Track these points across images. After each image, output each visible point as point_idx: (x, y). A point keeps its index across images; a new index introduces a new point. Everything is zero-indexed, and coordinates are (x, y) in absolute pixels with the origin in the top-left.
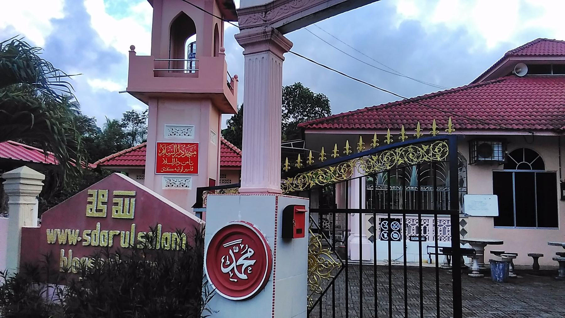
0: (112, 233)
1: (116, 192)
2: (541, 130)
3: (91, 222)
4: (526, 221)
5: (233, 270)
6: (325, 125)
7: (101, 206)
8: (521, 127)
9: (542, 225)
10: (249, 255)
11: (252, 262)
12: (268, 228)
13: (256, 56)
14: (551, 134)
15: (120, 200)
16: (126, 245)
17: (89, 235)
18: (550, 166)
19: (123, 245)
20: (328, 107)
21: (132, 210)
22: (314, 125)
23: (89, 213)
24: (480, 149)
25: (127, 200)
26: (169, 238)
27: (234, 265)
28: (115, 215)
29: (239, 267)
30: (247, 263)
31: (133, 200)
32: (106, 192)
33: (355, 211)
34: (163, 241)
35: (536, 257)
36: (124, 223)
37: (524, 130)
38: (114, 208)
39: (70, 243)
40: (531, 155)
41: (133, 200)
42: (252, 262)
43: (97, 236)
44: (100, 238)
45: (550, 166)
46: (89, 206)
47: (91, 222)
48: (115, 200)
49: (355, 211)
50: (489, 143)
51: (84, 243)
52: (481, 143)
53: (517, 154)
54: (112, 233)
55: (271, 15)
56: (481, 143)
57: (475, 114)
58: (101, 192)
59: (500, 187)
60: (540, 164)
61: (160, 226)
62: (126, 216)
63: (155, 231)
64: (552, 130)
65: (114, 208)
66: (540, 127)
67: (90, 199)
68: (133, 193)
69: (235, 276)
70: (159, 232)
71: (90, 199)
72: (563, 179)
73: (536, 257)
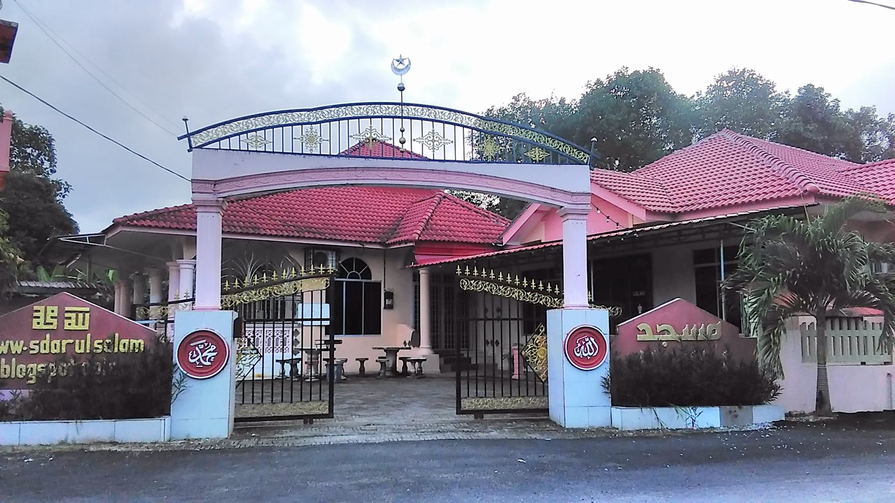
0: (64, 342)
1: (67, 309)
2: (370, 243)
3: (39, 334)
4: (354, 330)
5: (199, 360)
6: (149, 222)
7: (49, 320)
8: (354, 239)
9: (368, 332)
10: (212, 349)
11: (215, 354)
12: (225, 331)
13: (207, 214)
14: (378, 247)
15: (73, 315)
16: (82, 351)
17: (38, 344)
18: (376, 276)
19: (77, 351)
20: (52, 150)
21: (87, 323)
22: (135, 222)
23: (35, 326)
24: (315, 255)
25: (81, 315)
26: (127, 343)
27: (200, 356)
28: (67, 327)
29: (204, 358)
30: (210, 355)
31: (87, 315)
32: (55, 308)
33: (481, 319)
34: (121, 346)
35: (362, 361)
36: (81, 334)
37: (356, 242)
38: (67, 322)
39: (14, 352)
40: (361, 264)
41: (87, 315)
42: (215, 354)
43: (48, 345)
44: (57, 346)
45: (376, 276)
46: (35, 321)
47: (39, 334)
48: (67, 315)
49: (481, 319)
50: (324, 252)
51: (31, 352)
52: (316, 251)
53: (348, 263)
54: (64, 342)
55: (218, 187)
56: (316, 251)
57: (311, 220)
58: (49, 308)
59: (332, 296)
60: (368, 274)
61: (117, 335)
62: (80, 327)
63: (113, 339)
64: (379, 243)
65: (67, 322)
66: (369, 240)
67: (36, 314)
68: (88, 309)
69: (201, 364)
70: (117, 339)
71: (36, 314)
72: (387, 289)
73: (362, 361)
